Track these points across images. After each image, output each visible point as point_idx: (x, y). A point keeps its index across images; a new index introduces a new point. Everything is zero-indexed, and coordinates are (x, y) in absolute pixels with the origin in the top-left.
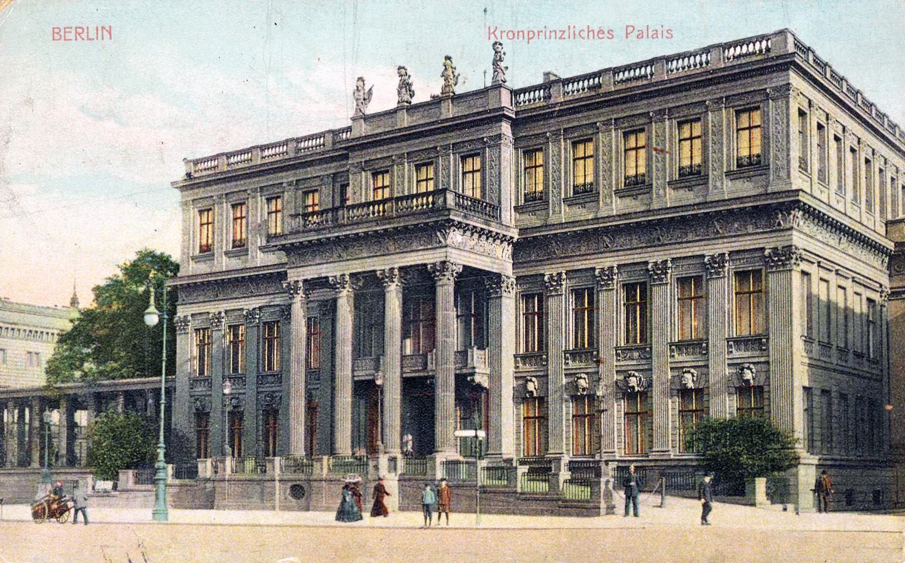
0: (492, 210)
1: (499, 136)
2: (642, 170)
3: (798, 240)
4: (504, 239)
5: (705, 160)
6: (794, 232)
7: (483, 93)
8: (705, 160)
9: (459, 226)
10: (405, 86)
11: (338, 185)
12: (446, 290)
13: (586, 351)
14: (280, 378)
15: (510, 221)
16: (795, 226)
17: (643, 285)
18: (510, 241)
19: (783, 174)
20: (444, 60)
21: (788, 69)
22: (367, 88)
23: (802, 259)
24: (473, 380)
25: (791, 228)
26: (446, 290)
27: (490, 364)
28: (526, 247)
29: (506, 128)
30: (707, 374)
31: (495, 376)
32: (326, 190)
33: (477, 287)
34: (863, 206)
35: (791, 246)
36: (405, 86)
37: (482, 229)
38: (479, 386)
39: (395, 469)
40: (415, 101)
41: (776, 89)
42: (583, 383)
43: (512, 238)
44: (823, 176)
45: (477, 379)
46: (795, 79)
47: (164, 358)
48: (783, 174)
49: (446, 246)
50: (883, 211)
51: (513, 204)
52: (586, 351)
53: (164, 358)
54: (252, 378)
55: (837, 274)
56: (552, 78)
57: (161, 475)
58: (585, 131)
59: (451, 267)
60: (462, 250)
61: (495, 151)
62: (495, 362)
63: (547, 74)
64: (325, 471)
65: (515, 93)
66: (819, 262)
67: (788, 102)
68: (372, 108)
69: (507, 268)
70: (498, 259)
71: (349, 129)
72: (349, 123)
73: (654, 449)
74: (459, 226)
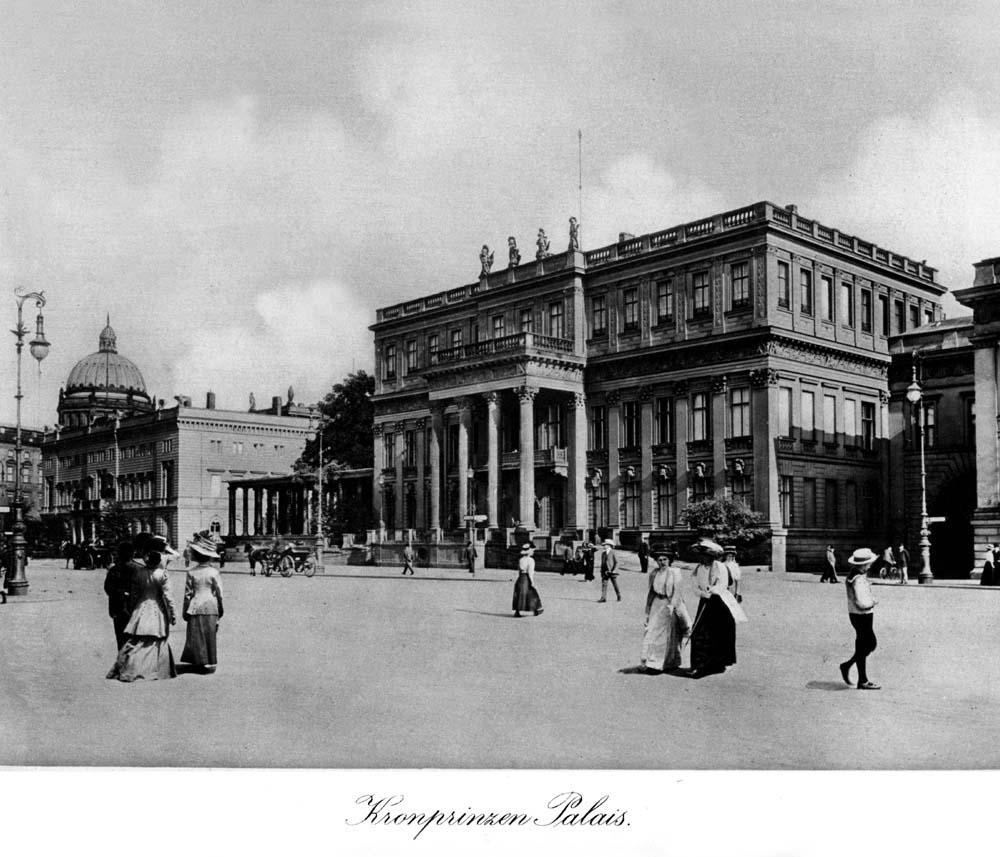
0: (568, 345)
1: (573, 289)
2: (670, 312)
3: (773, 363)
4: (575, 366)
5: (711, 303)
6: (770, 358)
7: (564, 256)
8: (711, 303)
9: (534, 359)
10: (514, 252)
11: (473, 326)
12: (527, 410)
13: (632, 452)
14: (783, 494)
15: (581, 353)
16: (771, 353)
17: (671, 398)
18: (581, 367)
19: (762, 313)
20: (538, 232)
21: (765, 233)
22: (490, 254)
23: (778, 377)
24: (554, 472)
25: (768, 355)
26: (527, 410)
27: (569, 461)
28: (593, 373)
29: (578, 282)
30: (712, 467)
31: (572, 469)
32: (466, 330)
33: (554, 407)
34: (859, 328)
35: (766, 370)
36: (514, 252)
37: (555, 361)
38: (559, 475)
39: (484, 538)
40: (521, 263)
41: (758, 248)
42: (631, 473)
43: (582, 365)
44: (808, 310)
45: (557, 470)
46: (771, 239)
47: (924, 472)
48: (762, 313)
49: (525, 375)
50: (886, 330)
51: (586, 339)
52: (632, 452)
53: (924, 472)
54: (399, 471)
55: (844, 389)
56: (627, 238)
57: (319, 542)
58: (741, 256)
59: (528, 390)
60: (539, 377)
61: (570, 300)
62: (571, 459)
63: (622, 235)
64: (438, 539)
65: (587, 255)
66: (800, 379)
67: (765, 259)
68: (494, 269)
69: (579, 389)
70: (574, 383)
71: (477, 285)
72: (478, 280)
73: (644, 524)
74: (534, 359)
